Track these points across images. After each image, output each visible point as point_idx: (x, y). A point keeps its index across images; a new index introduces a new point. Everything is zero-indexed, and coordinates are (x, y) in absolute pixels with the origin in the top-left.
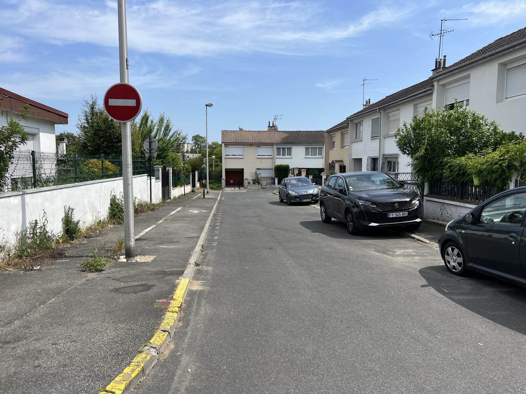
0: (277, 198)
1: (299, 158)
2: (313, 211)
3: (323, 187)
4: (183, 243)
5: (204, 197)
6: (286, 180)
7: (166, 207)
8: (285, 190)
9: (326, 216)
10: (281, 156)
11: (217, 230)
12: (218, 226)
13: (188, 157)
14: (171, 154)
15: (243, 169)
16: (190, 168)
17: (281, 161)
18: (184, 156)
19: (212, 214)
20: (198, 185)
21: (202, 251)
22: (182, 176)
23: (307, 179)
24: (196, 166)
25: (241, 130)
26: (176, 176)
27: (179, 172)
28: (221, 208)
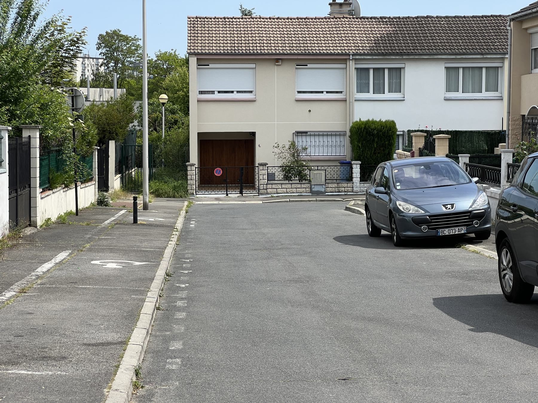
0: (359, 225)
1: (424, 100)
2: (472, 266)
3: (505, 188)
4: (78, 362)
5: (135, 220)
6: (388, 169)
7: (21, 252)
8: (385, 197)
9: (517, 279)
10: (370, 95)
11: (178, 321)
12: (179, 309)
13: (87, 98)
14: (37, 90)
15: (253, 134)
16: (94, 131)
17: (371, 109)
18: (74, 97)
19: (161, 273)
20: (115, 182)
21: (136, 386)
22: (70, 155)
23: (454, 165)
24: (110, 127)
25: (246, 14)
26: (53, 155)
27: (61, 144)
28: (188, 253)
